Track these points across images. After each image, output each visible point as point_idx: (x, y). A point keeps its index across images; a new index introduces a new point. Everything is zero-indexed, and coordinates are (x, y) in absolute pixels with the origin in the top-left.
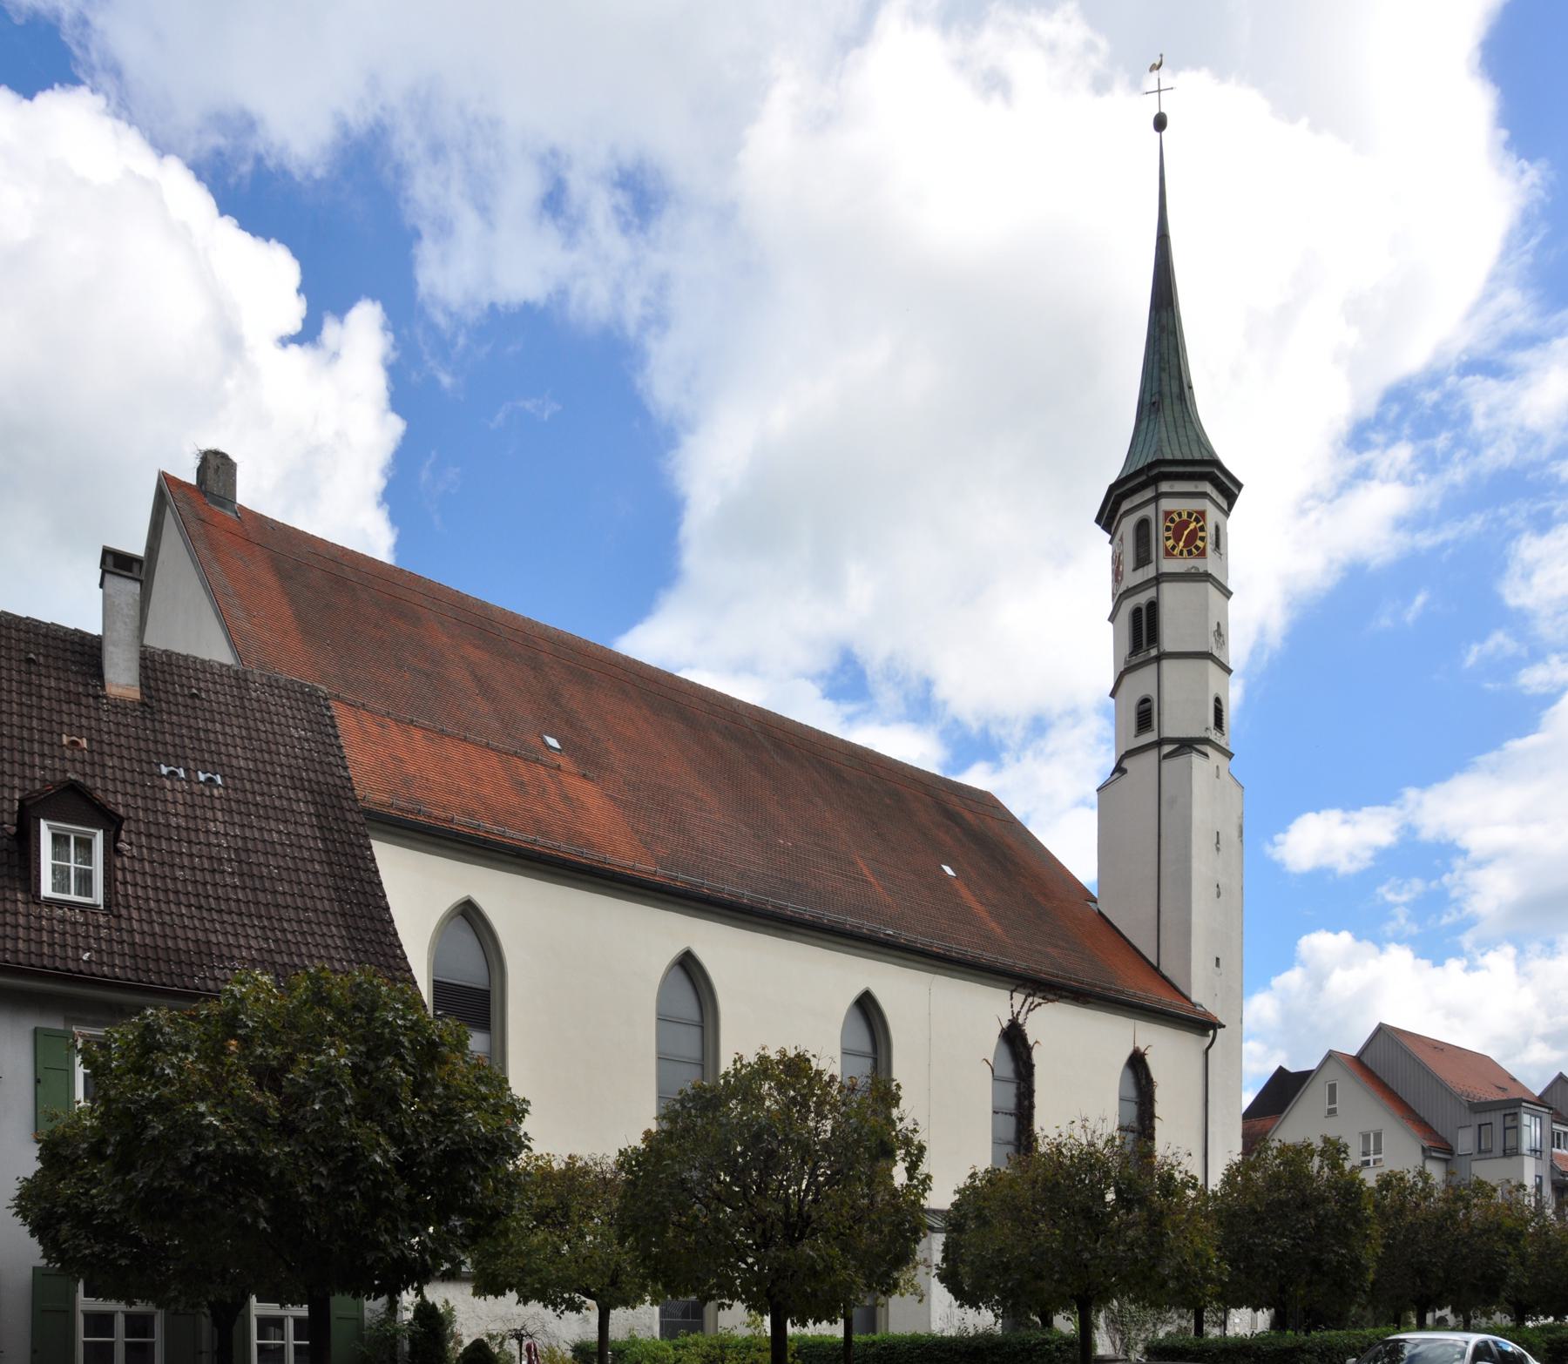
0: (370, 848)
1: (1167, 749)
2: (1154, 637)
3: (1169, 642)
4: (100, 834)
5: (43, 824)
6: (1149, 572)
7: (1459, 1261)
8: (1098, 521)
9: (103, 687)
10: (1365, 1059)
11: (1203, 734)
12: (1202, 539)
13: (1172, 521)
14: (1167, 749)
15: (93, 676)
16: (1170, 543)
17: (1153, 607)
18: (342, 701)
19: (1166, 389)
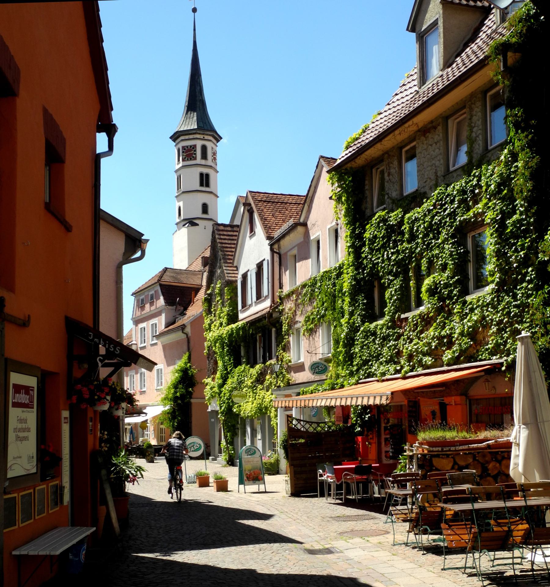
13: (185, 149)
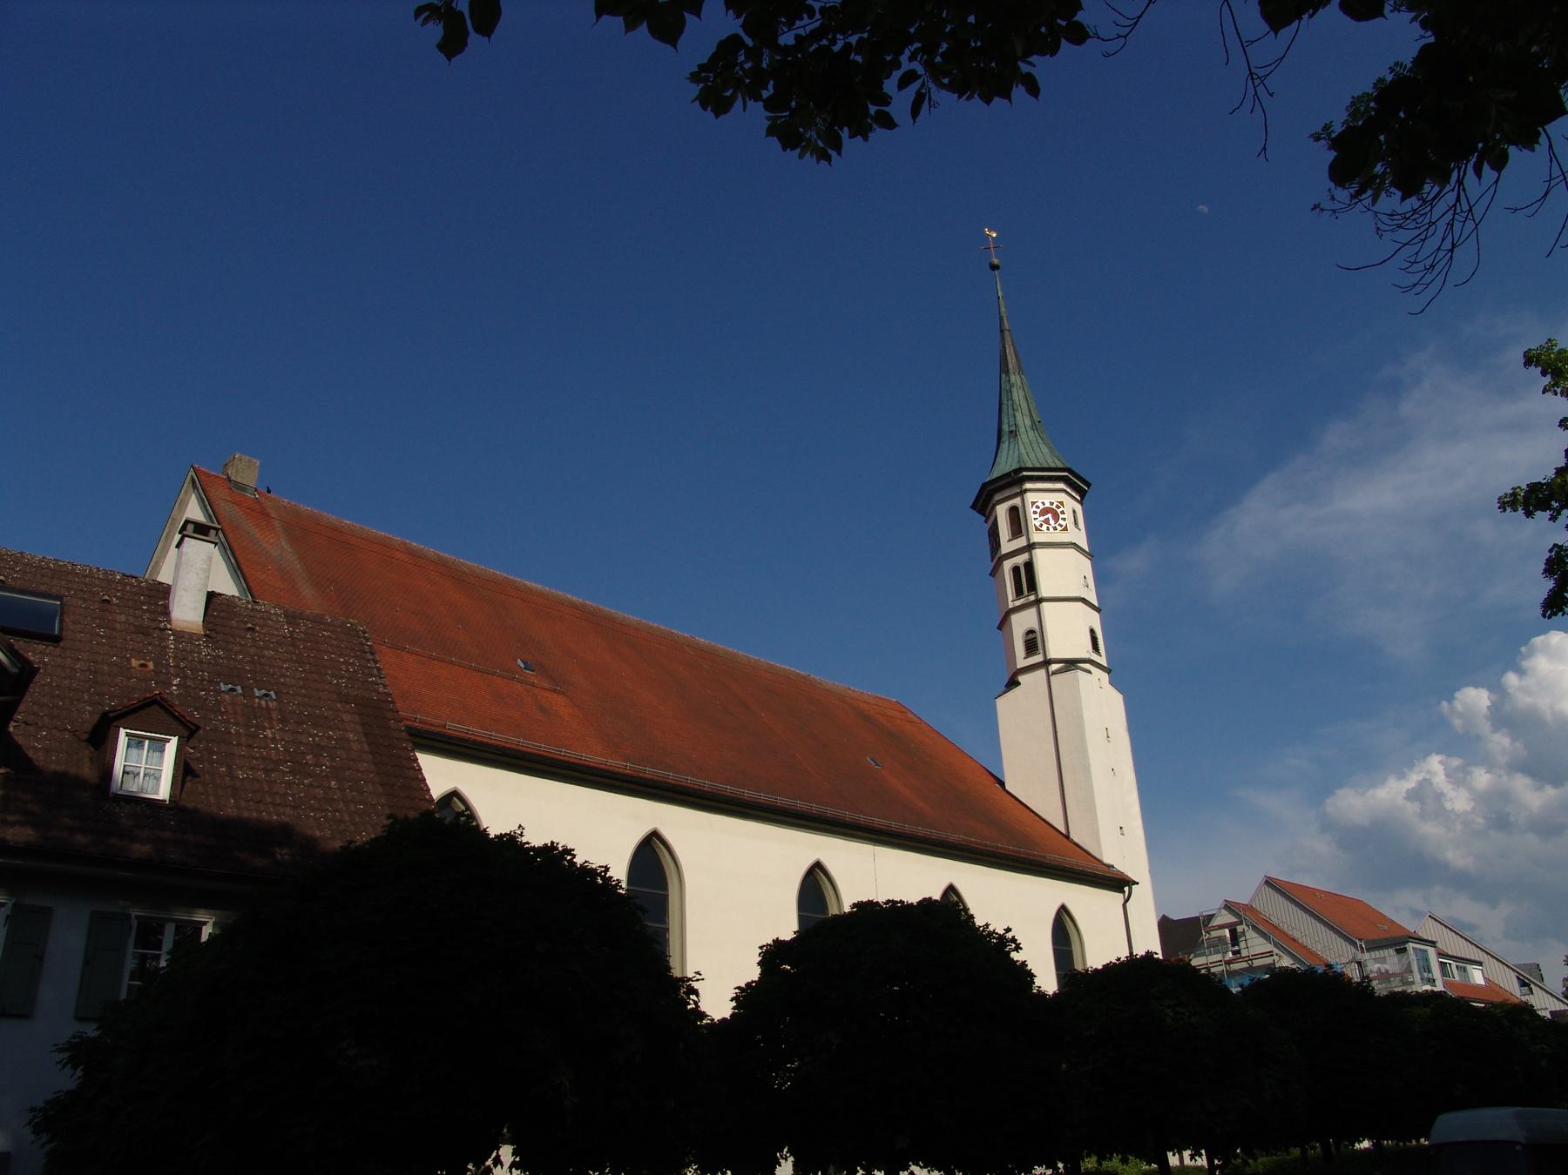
1: (1054, 667)
2: (1033, 586)
3: (1044, 590)
4: (174, 740)
5: (123, 732)
6: (1021, 542)
7: (1478, 1043)
8: (973, 507)
9: (169, 621)
11: (1086, 656)
14: (1054, 667)
15: (161, 614)
17: (1029, 566)
19: (1020, 423)
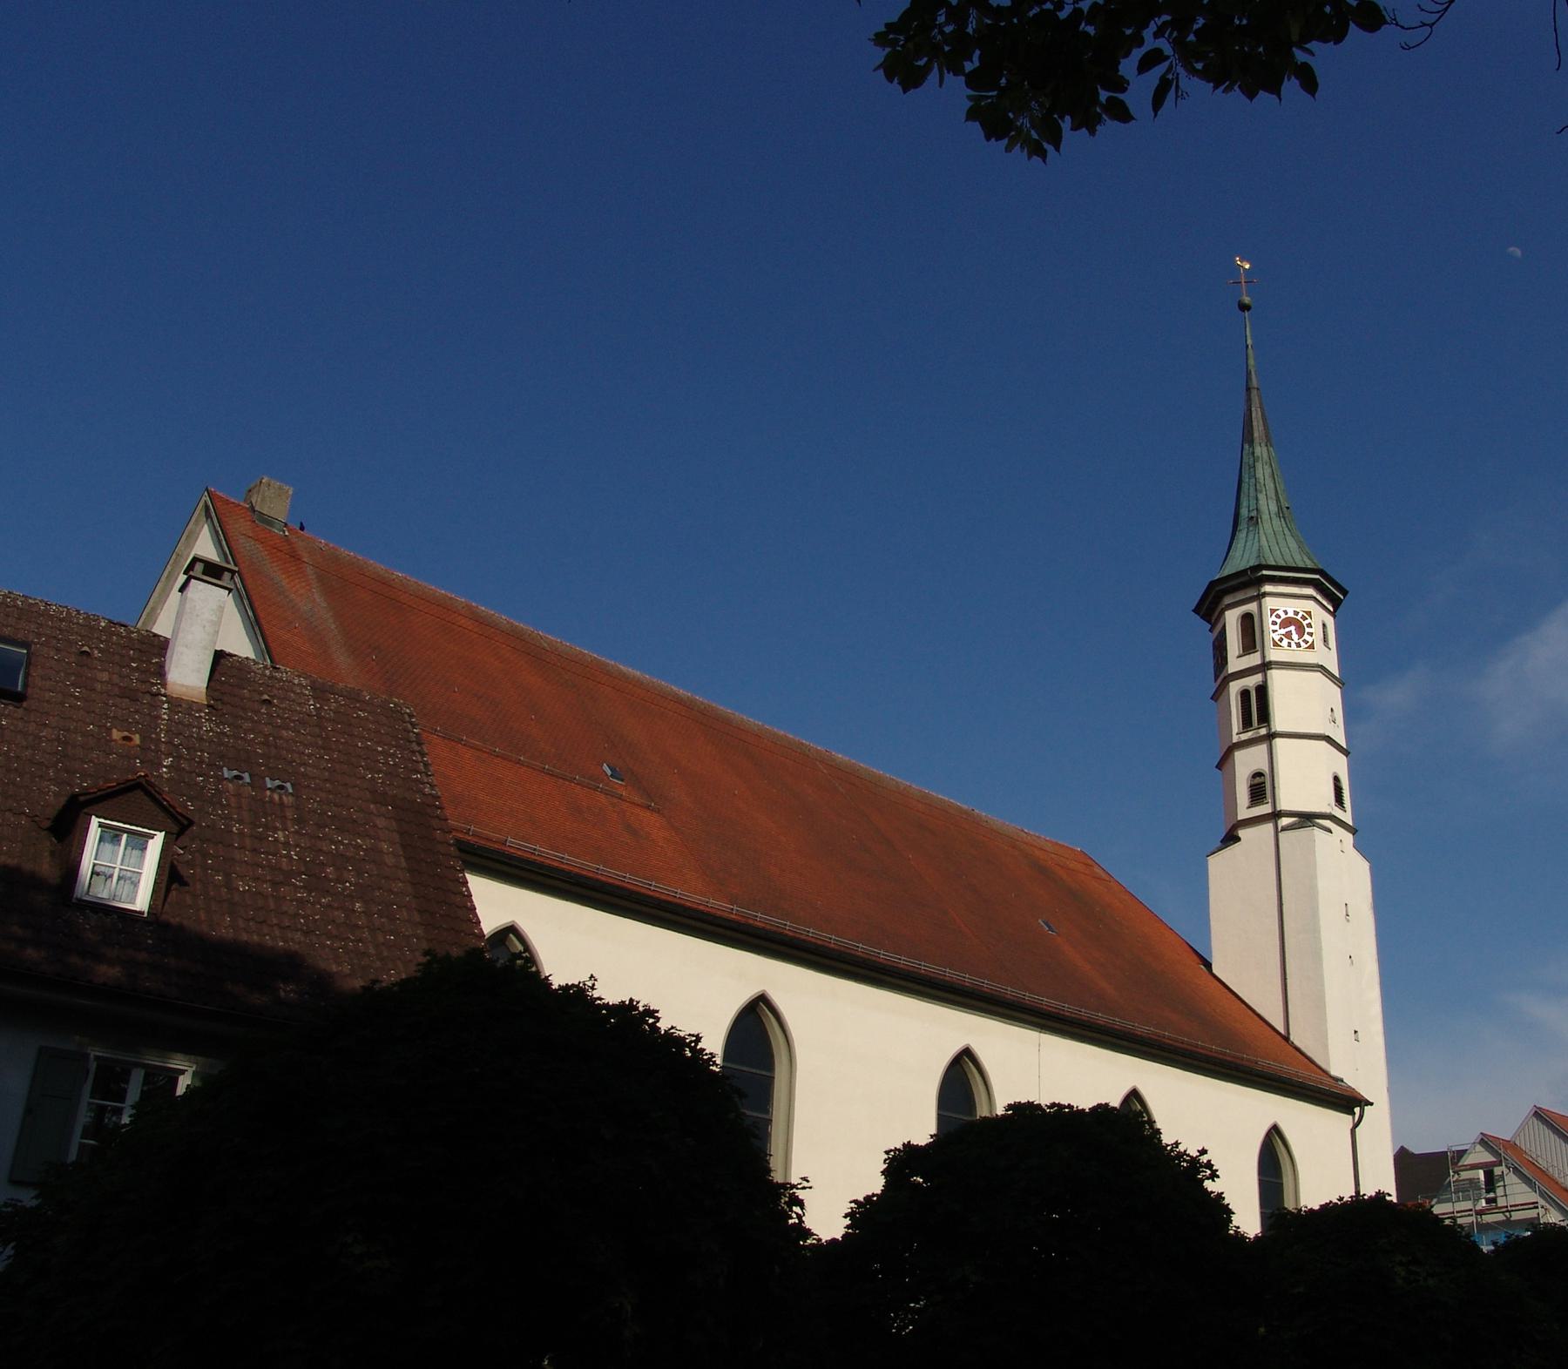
0: (466, 883)
1: (1285, 821)
2: (1265, 717)
3: (1279, 722)
5: (95, 821)
6: (1254, 659)
9: (164, 685)
10: (1345, 1120)
12: (1311, 634)
16: (1281, 613)
17: (1262, 690)
18: (1517, 1171)
19: (1263, 508)
